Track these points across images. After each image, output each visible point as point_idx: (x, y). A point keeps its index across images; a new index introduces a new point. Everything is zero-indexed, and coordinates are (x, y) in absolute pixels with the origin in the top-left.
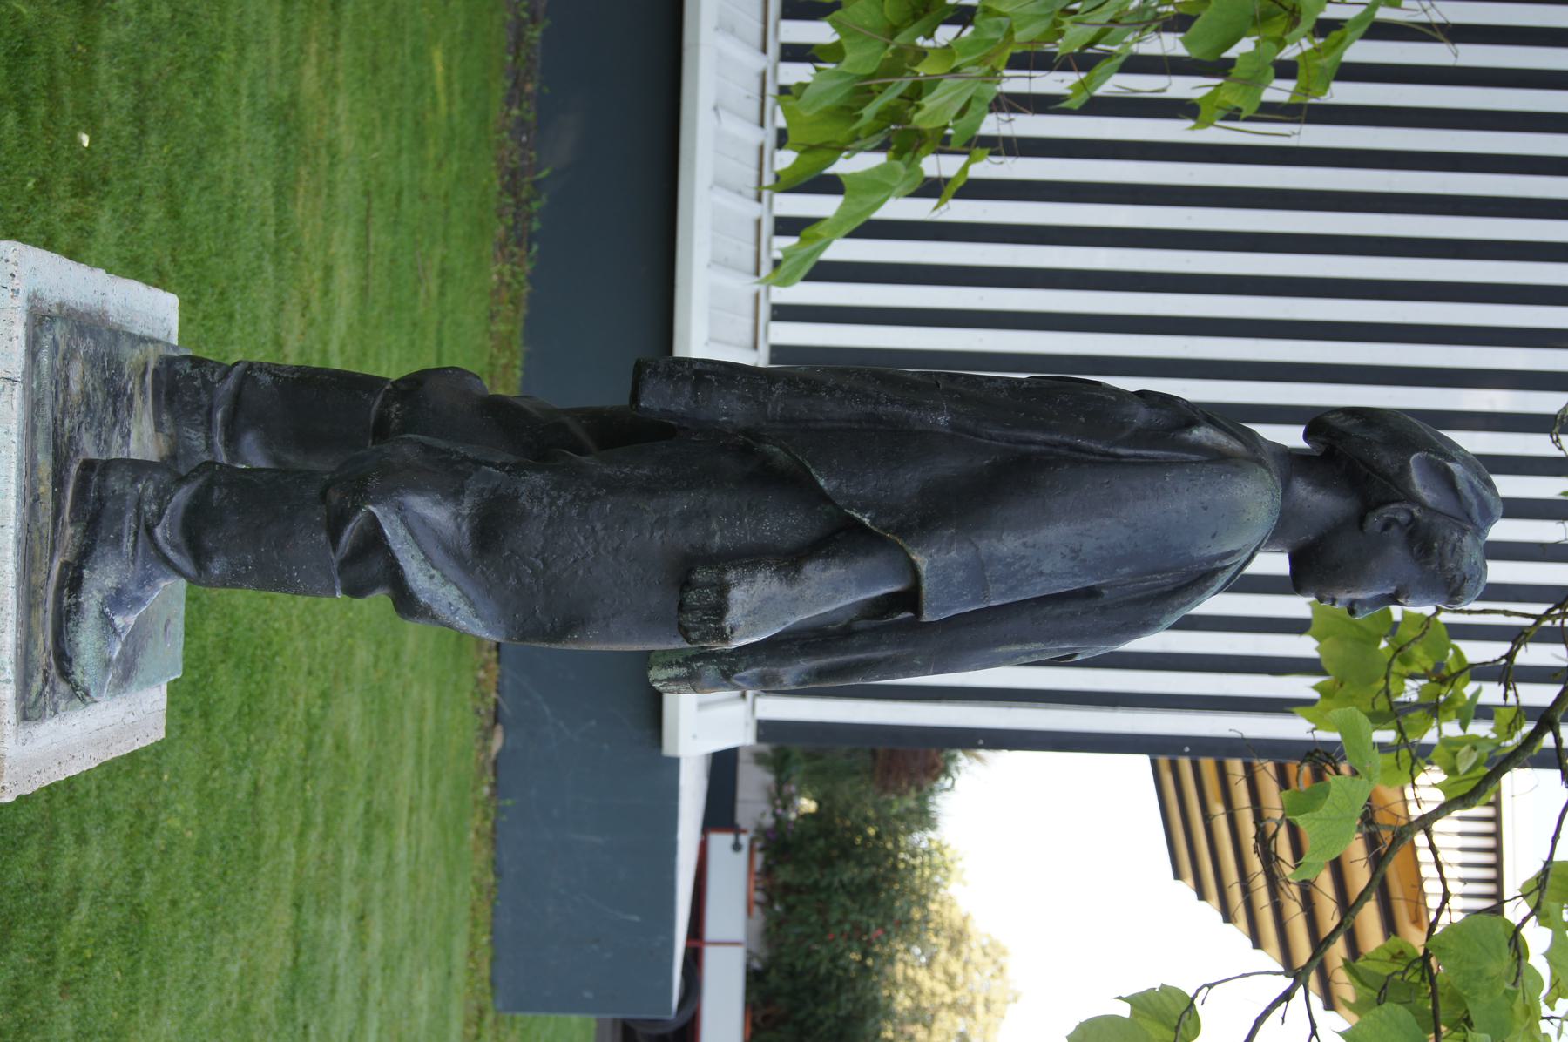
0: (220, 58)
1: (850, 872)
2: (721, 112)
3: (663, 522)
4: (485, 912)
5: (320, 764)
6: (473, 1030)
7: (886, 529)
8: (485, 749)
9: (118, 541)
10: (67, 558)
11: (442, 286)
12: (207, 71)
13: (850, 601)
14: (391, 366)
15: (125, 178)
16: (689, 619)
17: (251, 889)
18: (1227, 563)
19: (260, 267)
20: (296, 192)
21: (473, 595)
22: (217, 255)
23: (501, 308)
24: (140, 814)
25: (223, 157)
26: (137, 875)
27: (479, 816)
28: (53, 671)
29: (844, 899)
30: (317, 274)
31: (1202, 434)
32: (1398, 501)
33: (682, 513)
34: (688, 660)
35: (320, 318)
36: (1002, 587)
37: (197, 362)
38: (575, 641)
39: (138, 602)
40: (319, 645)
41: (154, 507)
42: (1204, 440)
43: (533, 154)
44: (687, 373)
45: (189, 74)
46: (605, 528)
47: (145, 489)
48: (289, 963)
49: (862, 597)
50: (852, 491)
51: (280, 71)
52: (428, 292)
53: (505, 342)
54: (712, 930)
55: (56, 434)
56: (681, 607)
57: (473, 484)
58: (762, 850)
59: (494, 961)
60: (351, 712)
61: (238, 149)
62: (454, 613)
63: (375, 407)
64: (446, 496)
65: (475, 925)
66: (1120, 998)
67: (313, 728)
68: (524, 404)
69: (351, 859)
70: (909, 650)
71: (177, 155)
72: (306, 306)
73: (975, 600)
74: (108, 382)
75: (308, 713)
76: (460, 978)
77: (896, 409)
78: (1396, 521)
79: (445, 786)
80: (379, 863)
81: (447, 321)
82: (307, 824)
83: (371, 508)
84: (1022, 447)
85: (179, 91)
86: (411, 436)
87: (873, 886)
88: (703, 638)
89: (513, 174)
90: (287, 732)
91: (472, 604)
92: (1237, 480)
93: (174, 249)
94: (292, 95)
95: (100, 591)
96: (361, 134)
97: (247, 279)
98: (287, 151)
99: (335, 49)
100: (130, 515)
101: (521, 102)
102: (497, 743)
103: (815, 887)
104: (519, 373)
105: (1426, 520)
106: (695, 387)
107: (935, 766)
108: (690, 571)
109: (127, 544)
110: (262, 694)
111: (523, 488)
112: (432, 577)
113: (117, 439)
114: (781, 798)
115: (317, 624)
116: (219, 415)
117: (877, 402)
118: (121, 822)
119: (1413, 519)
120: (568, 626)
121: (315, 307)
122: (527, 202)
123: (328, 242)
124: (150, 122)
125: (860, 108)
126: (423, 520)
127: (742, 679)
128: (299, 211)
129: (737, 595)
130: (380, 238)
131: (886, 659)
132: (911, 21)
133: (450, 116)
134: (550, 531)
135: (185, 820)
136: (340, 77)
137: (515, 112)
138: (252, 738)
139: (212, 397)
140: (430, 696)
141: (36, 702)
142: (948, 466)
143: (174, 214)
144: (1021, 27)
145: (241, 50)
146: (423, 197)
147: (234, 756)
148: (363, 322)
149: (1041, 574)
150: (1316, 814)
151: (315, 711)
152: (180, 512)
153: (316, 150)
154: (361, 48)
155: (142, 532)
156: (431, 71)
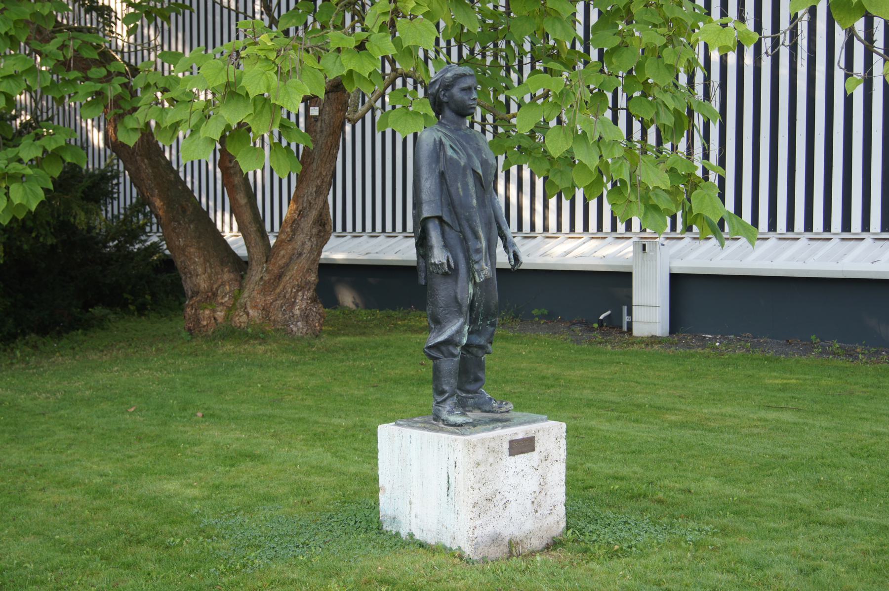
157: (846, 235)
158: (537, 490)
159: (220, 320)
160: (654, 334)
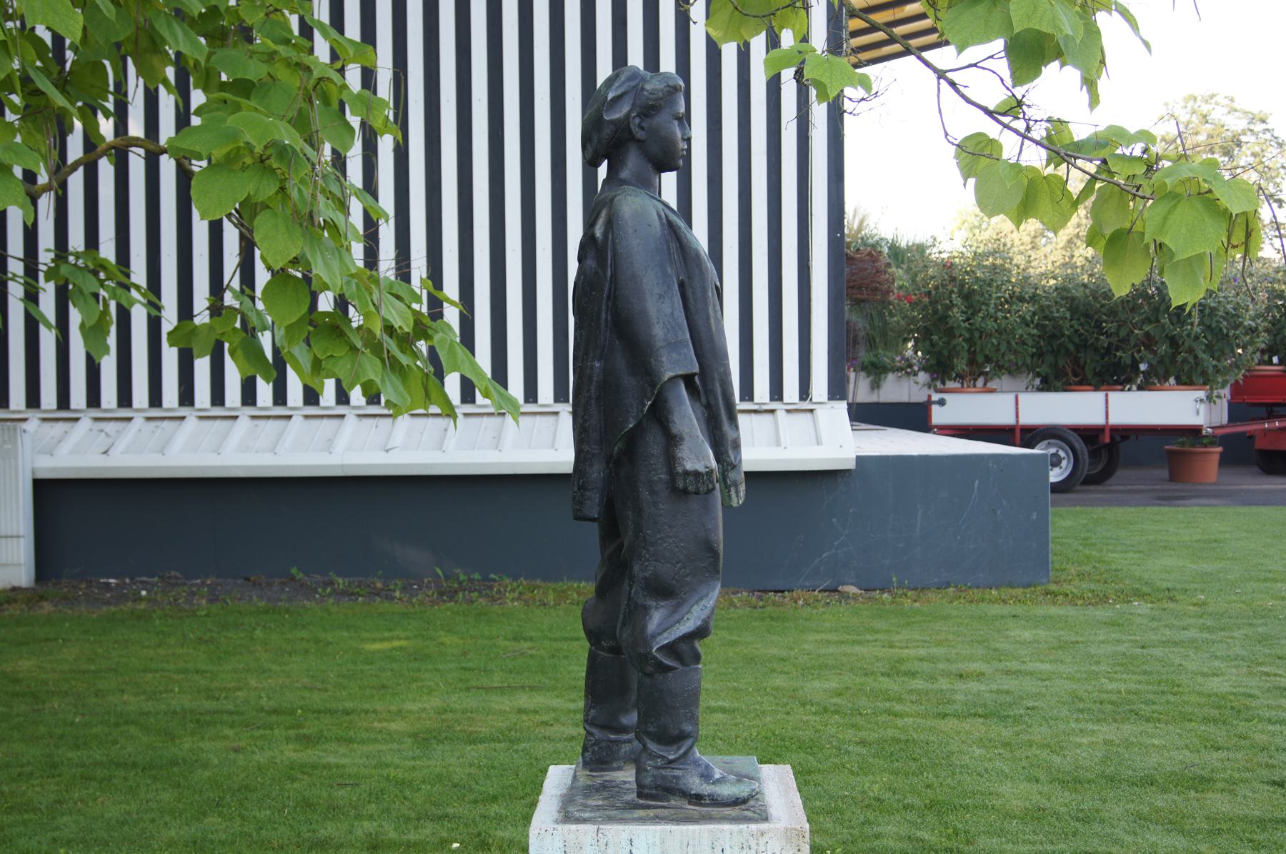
0: (394, 777)
1: (957, 314)
2: (388, 447)
3: (655, 504)
4: (976, 594)
5: (849, 705)
6: (1061, 598)
7: (653, 393)
8: (855, 597)
9: (677, 777)
10: (686, 802)
11: (525, 639)
12: (400, 783)
13: (690, 409)
14: (581, 649)
15: (476, 825)
16: (703, 489)
17: (927, 743)
18: (663, 216)
19: (523, 751)
20: (471, 733)
21: (697, 598)
22: (517, 775)
23: (537, 599)
24: (868, 806)
25: (455, 773)
26: (906, 807)
27: (903, 600)
28: (743, 807)
29: (978, 319)
30: (524, 717)
31: (598, 231)
32: (629, 123)
33: (650, 494)
34: (727, 487)
35: (553, 715)
36: (680, 333)
37: (585, 749)
38: (718, 546)
39: (707, 766)
40: (770, 709)
41: (659, 760)
42: (602, 231)
43: (426, 581)
44: (579, 494)
45: (408, 793)
46: (659, 532)
47: (650, 766)
48: (982, 720)
49: (688, 402)
50: (635, 410)
51: (395, 744)
52: (530, 649)
53: (562, 596)
54: (1006, 418)
55: (624, 809)
56: (697, 493)
57: (641, 601)
58: (943, 383)
59: (1011, 586)
60: (817, 687)
61: (450, 765)
62: (706, 607)
63: (605, 655)
64: (647, 614)
65: (983, 600)
66: (965, 185)
67: (825, 710)
68: (599, 577)
69: (918, 684)
70: (716, 375)
71: (458, 799)
72: (546, 724)
73: (687, 346)
74: (597, 790)
75: (815, 714)
76: (1019, 609)
77: (593, 388)
78: (639, 124)
79: (879, 624)
80: (925, 666)
81: (550, 635)
82: (889, 712)
83: (654, 650)
84: (609, 324)
85: (419, 799)
86: (618, 632)
87: (967, 296)
88: (712, 482)
89: (441, 594)
90: (826, 725)
91: (701, 599)
92: (621, 214)
93: (516, 798)
94: (410, 737)
95: (702, 785)
96: (428, 694)
97: (531, 758)
98: (446, 738)
99: (375, 712)
100: (663, 772)
101: (390, 590)
102: (852, 589)
103: (970, 341)
104: (583, 584)
105: (638, 109)
106: (586, 490)
107: (870, 254)
108: (678, 489)
109: (677, 773)
110: (799, 741)
111: (641, 575)
112: (688, 619)
113: (627, 786)
114: (906, 369)
115: (757, 710)
116: (612, 736)
117: (590, 398)
118: (871, 816)
119: (638, 115)
120: (712, 551)
121: (545, 718)
122: (460, 583)
123: (502, 712)
124: (440, 813)
125: (403, 366)
126: (659, 625)
127: (735, 459)
128: (484, 730)
129: (689, 466)
130: (497, 680)
131: (721, 386)
132: (346, 338)
133: (407, 638)
134: (662, 561)
135: (874, 782)
136: (393, 708)
137: (397, 594)
138: (827, 746)
139: (603, 741)
140: (812, 637)
141: (758, 814)
142: (620, 362)
143: (494, 799)
144: (348, 270)
145: (387, 766)
146: (465, 654)
147: (837, 756)
148: (554, 688)
149: (672, 313)
150: (828, 86)
151: (813, 709)
152: (661, 747)
153: (443, 721)
154: (372, 696)
155: (671, 766)
156: (379, 651)
157: (312, 410)
160: (16, 584)
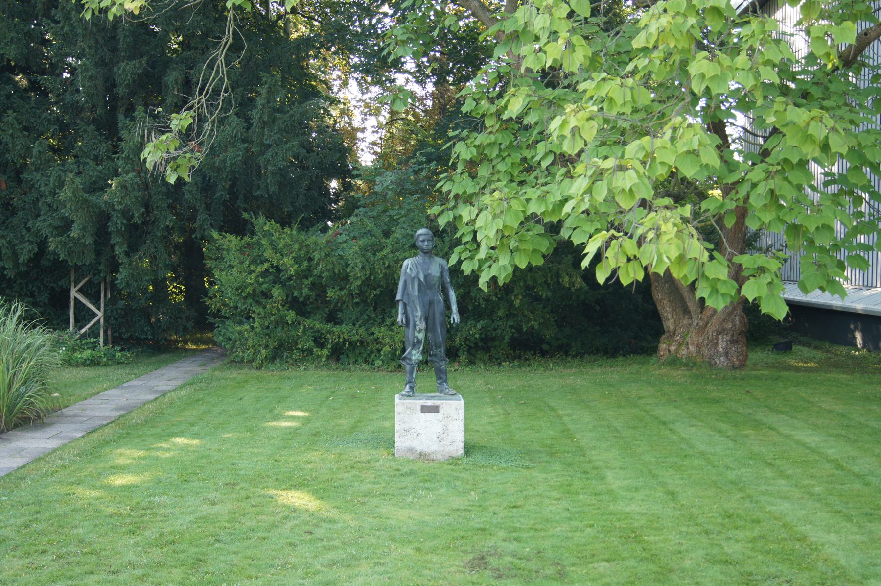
158: (442, 432)
159: (672, 352)
